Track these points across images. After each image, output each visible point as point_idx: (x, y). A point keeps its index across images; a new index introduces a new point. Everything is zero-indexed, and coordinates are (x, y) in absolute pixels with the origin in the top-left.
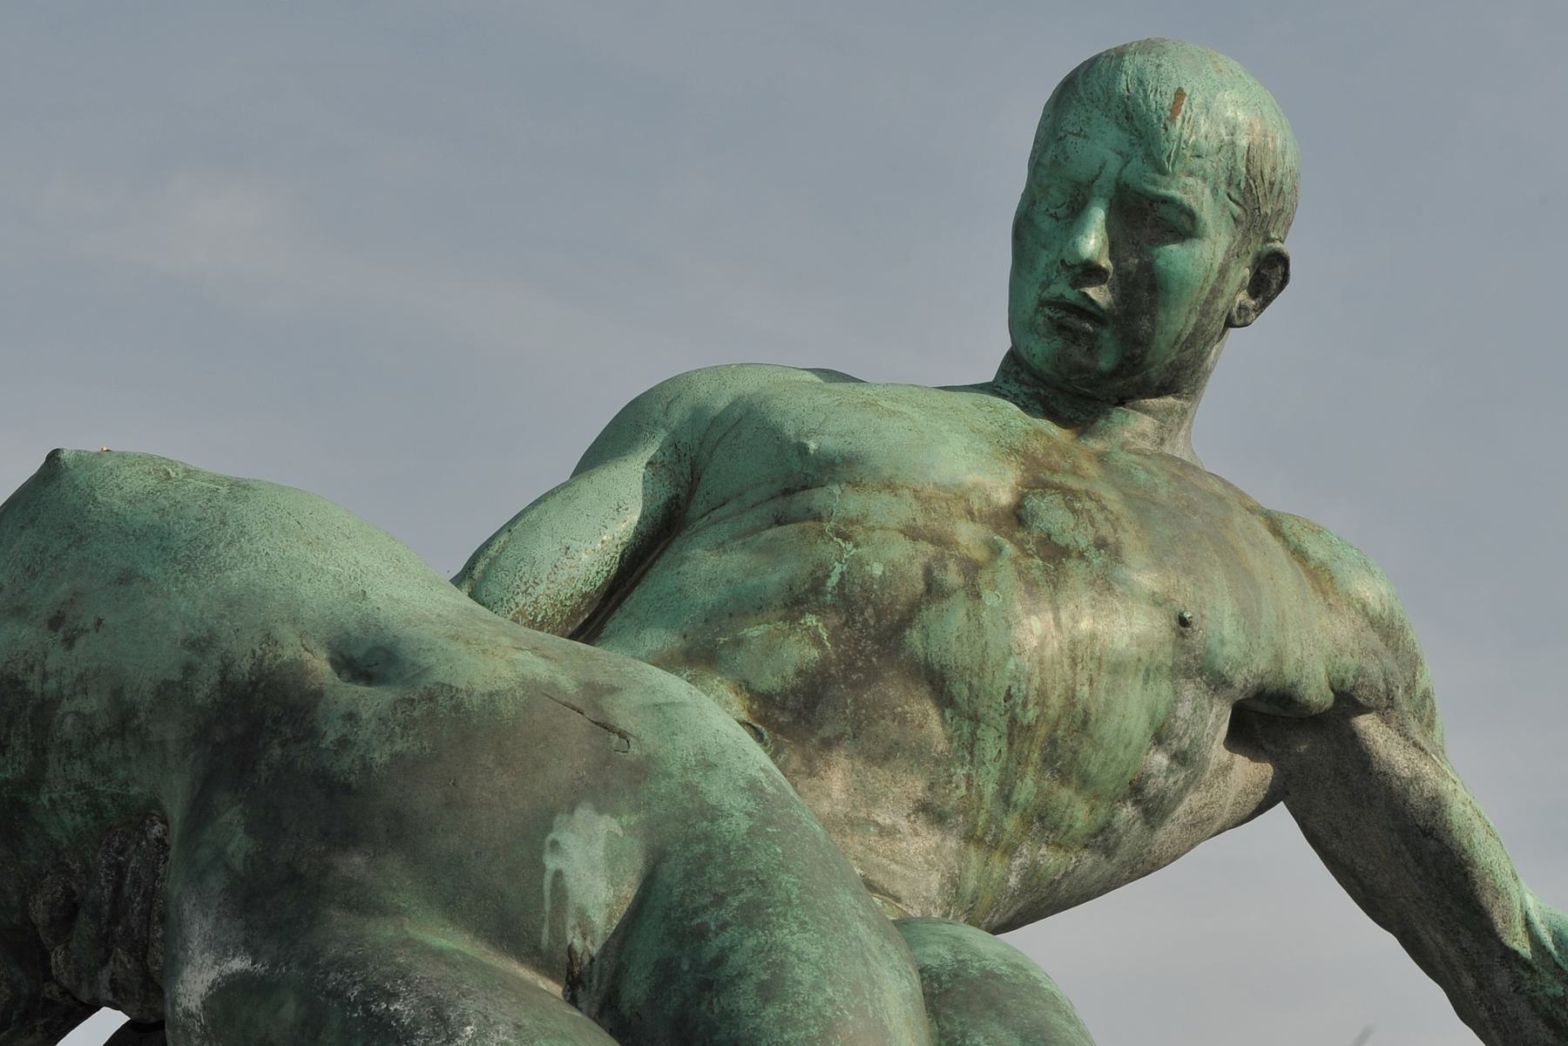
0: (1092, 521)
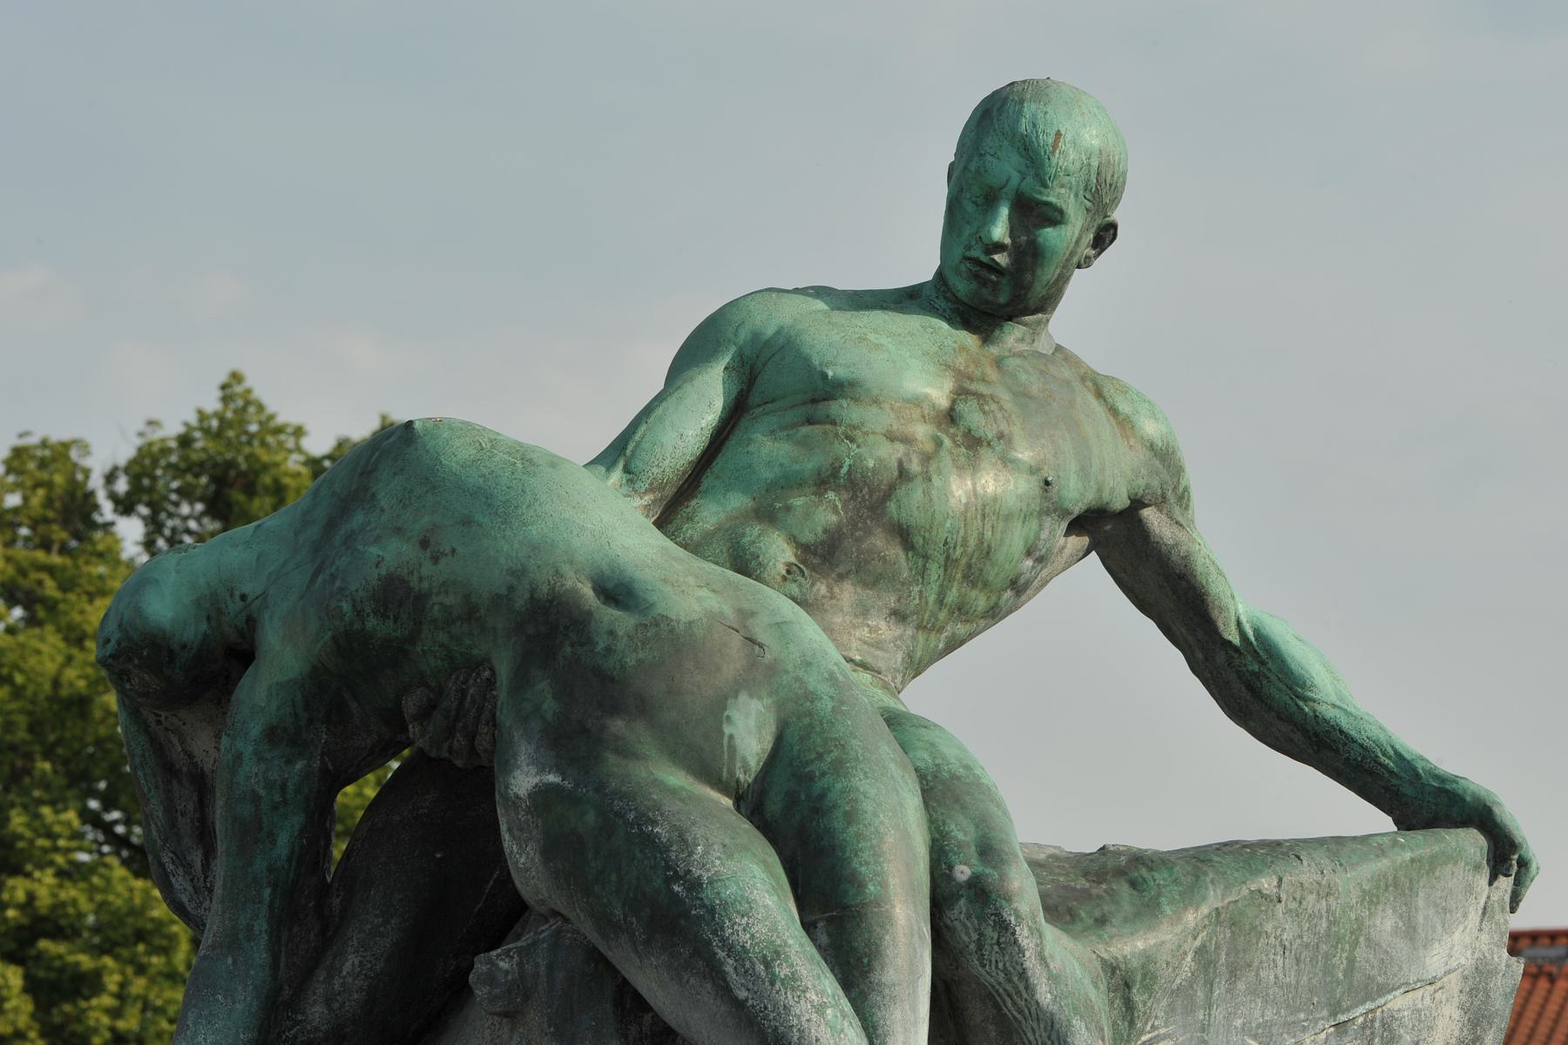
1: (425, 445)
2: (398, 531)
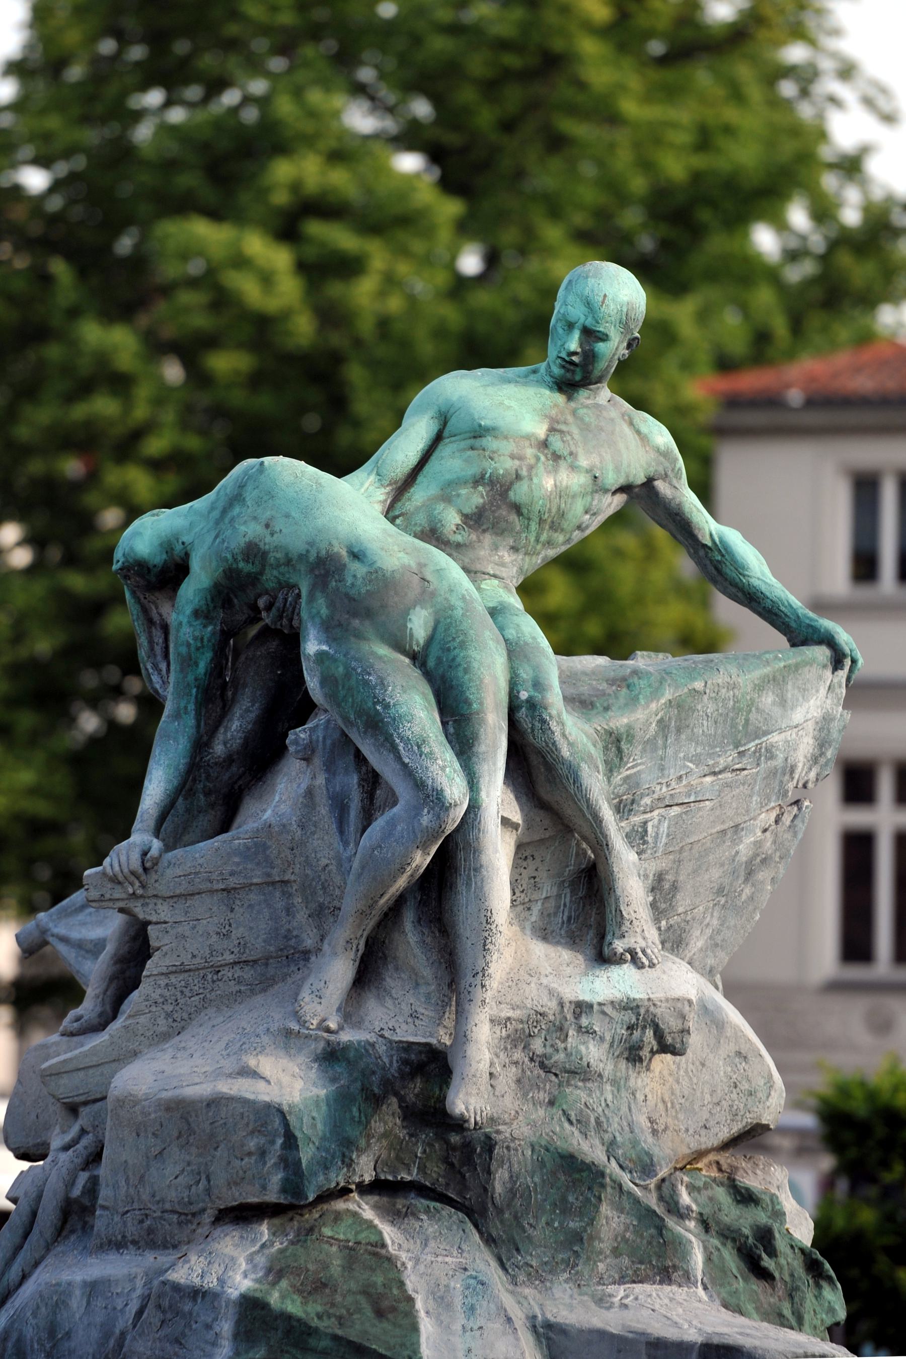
0: (569, 445)
1: (269, 475)
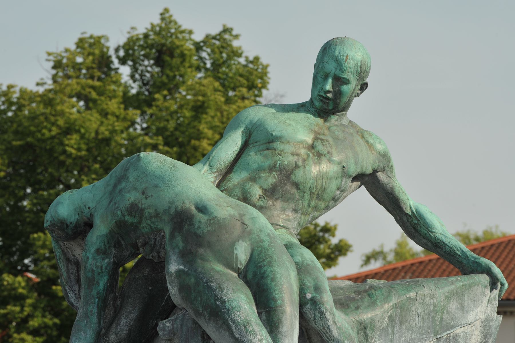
2: (135, 189)
